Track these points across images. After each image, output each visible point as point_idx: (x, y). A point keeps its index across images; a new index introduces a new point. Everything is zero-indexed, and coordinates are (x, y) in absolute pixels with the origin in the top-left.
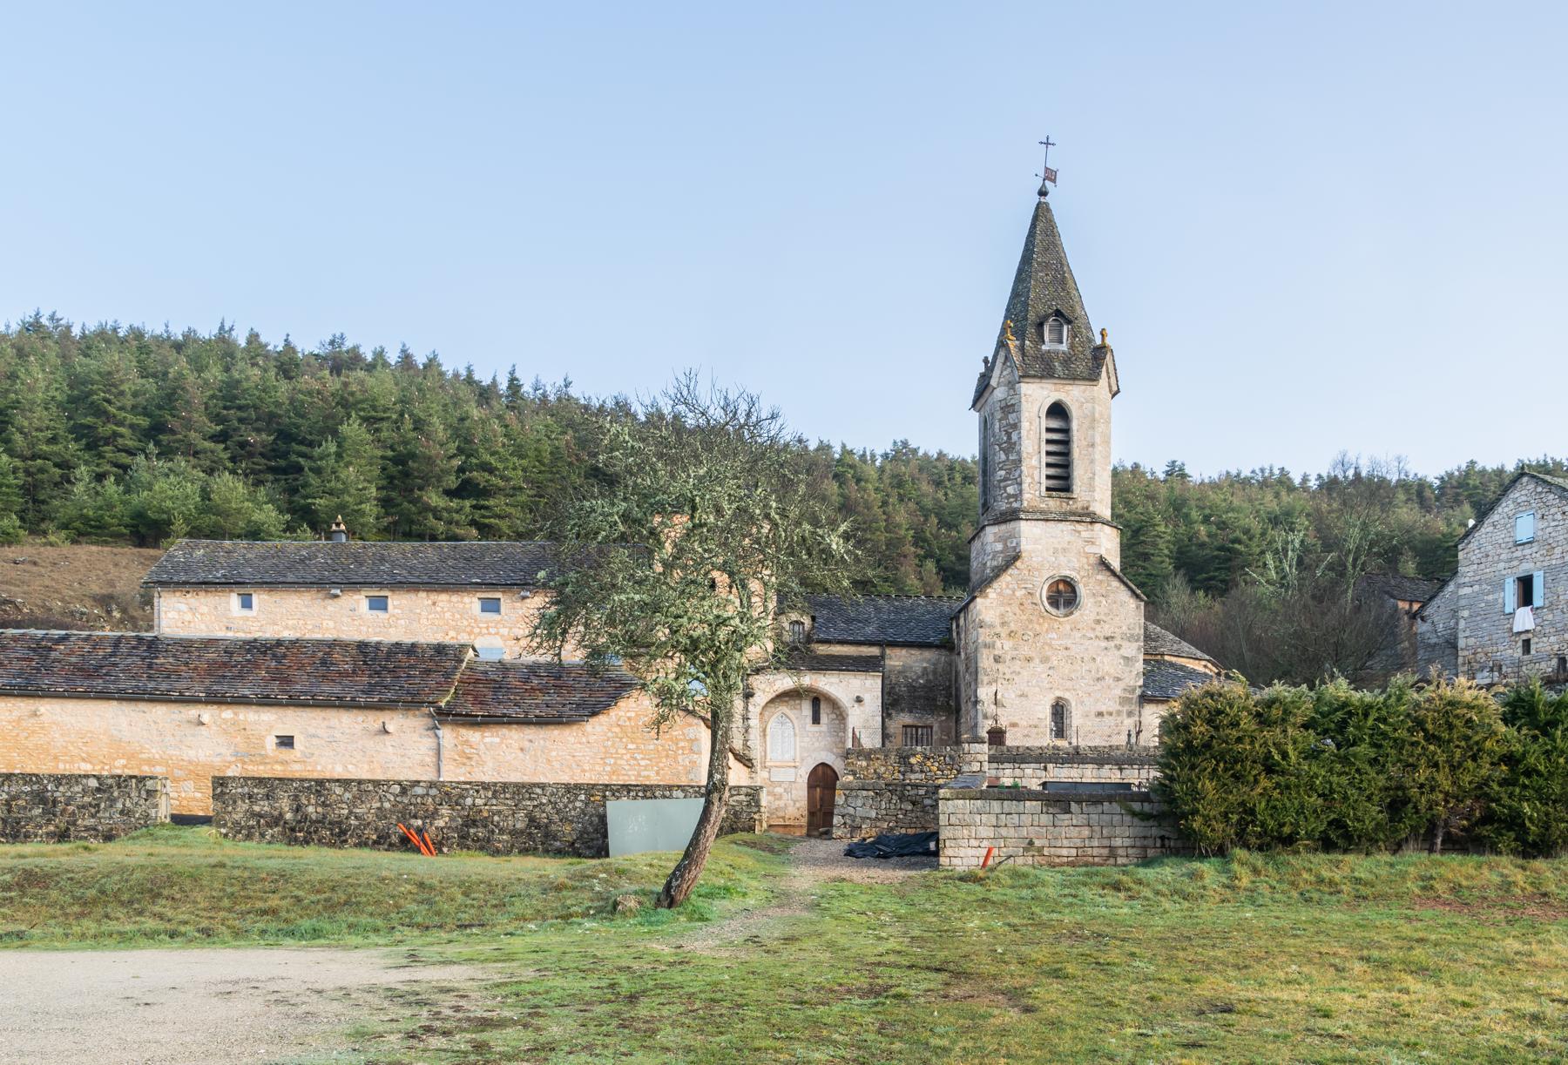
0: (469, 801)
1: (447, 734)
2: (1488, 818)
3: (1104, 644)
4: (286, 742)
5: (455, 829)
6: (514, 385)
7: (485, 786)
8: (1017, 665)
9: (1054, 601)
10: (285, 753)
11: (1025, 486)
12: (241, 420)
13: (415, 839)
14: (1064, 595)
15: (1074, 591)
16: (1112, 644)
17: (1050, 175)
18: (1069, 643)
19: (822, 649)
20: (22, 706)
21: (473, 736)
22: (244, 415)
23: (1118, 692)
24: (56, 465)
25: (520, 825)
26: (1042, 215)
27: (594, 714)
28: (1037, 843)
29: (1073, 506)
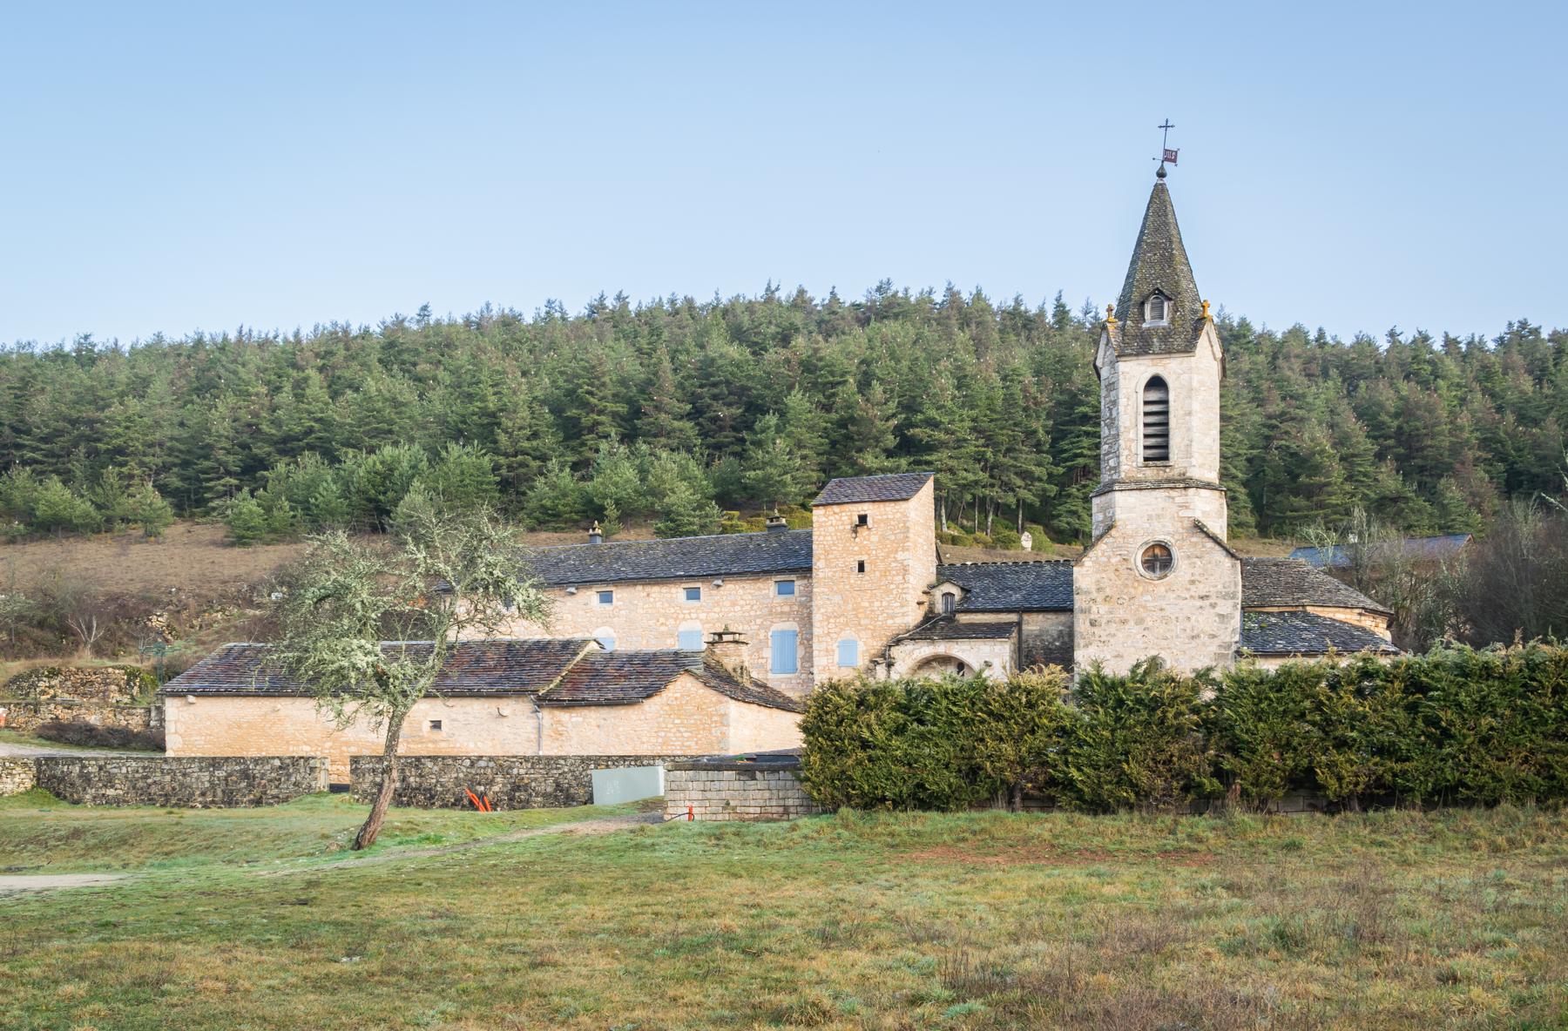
0: (515, 771)
1: (547, 715)
2: (1052, 782)
3: (1199, 603)
4: (437, 725)
5: (506, 793)
6: (1061, 312)
7: (526, 759)
8: (1113, 628)
9: (1150, 564)
10: (436, 735)
11: (1122, 459)
12: (715, 397)
13: (476, 801)
14: (1159, 559)
15: (1170, 554)
16: (1207, 602)
17: (1170, 156)
18: (1163, 604)
19: (964, 618)
20: (267, 704)
21: (564, 716)
22: (716, 391)
23: (1214, 648)
24: (535, 458)
25: (549, 790)
26: (1159, 202)
27: (649, 696)
28: (732, 803)
29: (1170, 473)
